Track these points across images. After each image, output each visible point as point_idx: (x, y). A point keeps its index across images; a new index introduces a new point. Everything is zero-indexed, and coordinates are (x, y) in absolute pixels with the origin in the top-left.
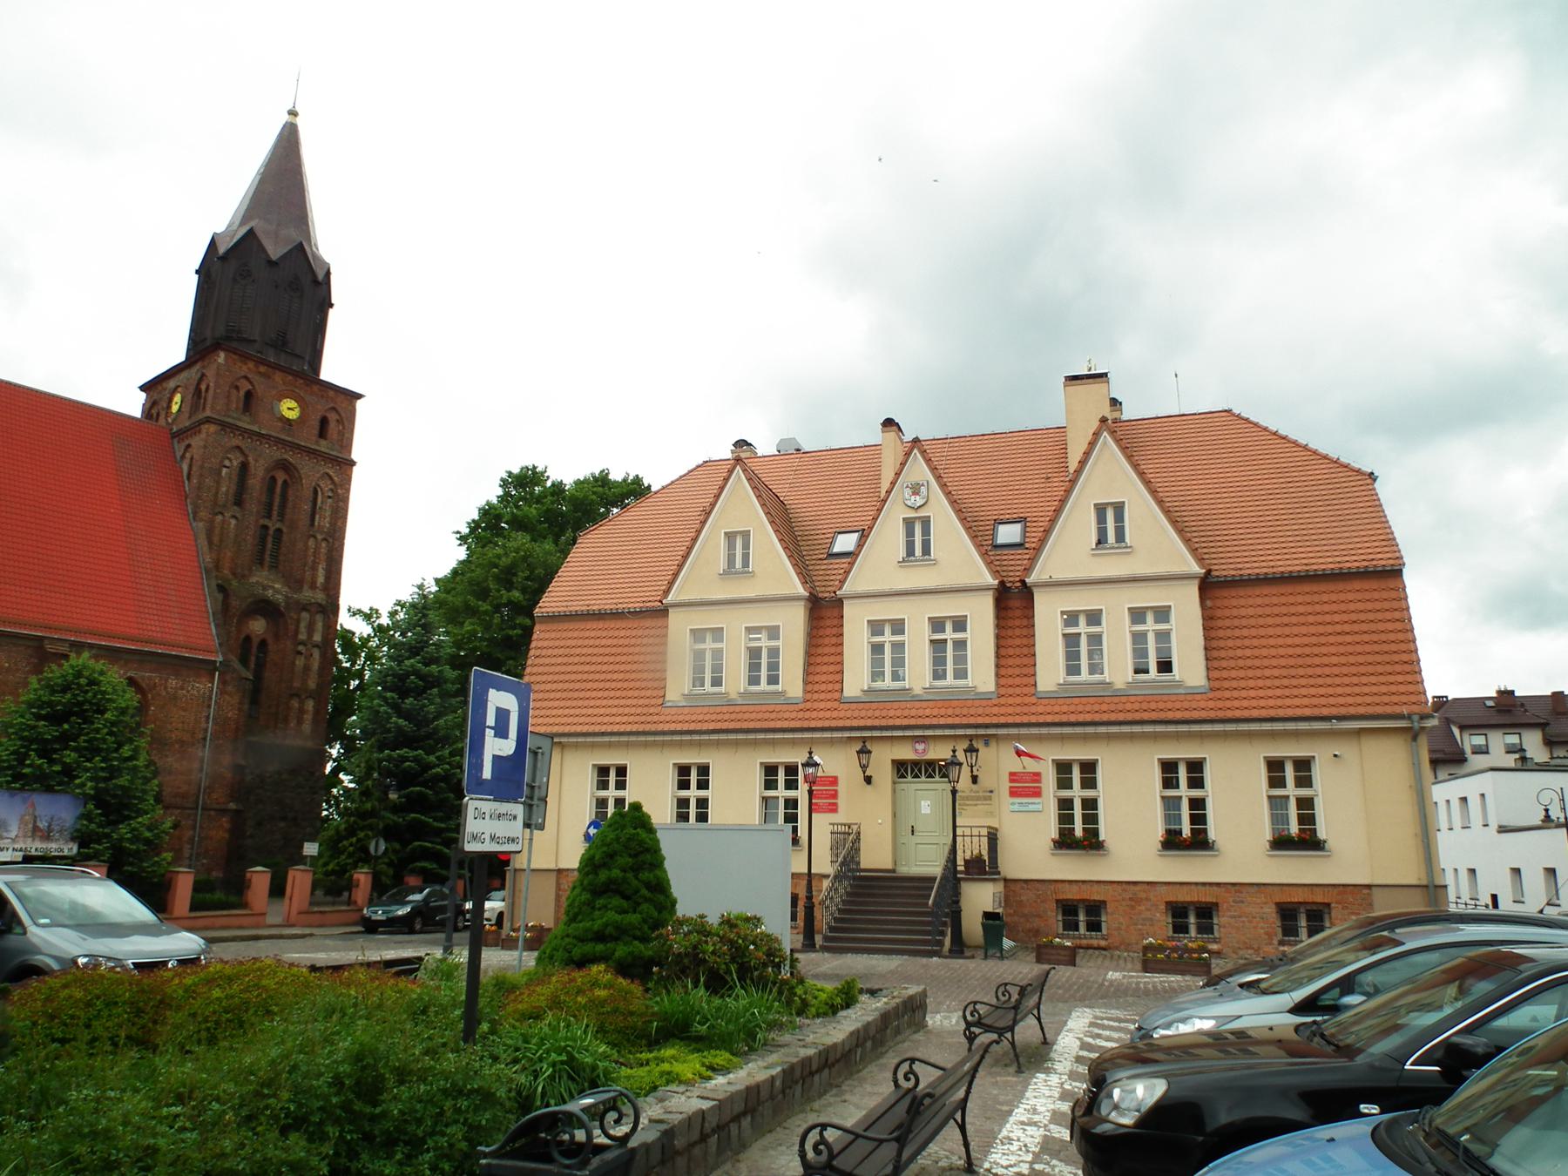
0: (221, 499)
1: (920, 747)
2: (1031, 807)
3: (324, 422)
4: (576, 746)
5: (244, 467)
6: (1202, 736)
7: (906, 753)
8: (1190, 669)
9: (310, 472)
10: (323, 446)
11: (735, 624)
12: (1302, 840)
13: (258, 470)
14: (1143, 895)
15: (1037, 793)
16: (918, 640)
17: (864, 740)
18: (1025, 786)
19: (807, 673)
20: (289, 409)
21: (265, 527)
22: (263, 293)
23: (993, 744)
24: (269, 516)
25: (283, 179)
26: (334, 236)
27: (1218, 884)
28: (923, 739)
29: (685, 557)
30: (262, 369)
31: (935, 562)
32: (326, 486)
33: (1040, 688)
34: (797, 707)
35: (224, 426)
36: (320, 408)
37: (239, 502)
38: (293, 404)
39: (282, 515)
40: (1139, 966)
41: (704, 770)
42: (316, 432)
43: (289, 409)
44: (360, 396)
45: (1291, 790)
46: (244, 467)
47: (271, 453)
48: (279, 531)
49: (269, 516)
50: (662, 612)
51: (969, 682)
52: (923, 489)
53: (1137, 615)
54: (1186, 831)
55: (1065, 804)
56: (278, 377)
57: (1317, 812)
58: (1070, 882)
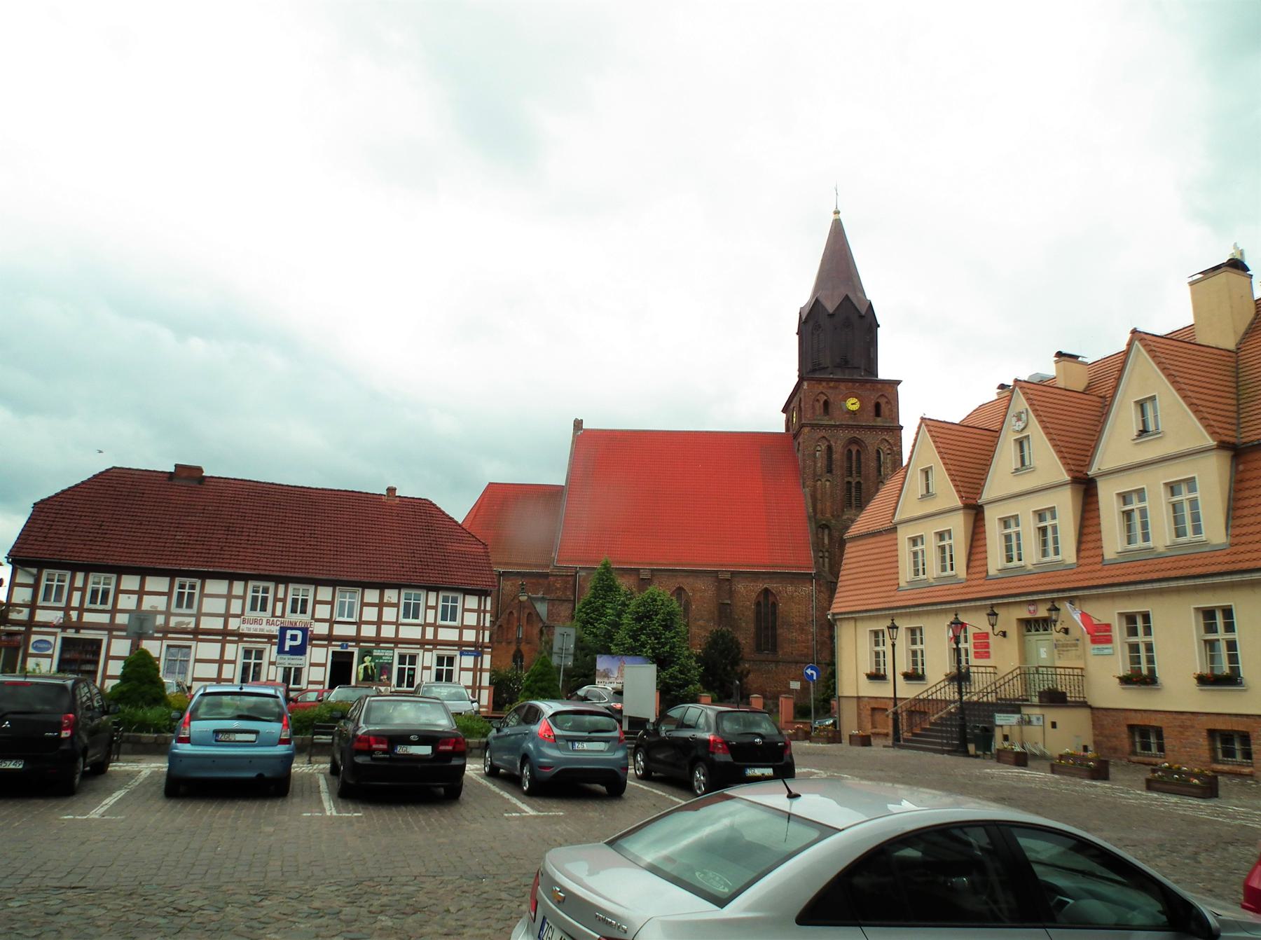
0: (819, 471)
1: (1032, 608)
2: (1106, 651)
3: (877, 407)
4: (863, 619)
5: (829, 448)
6: (918, 614)
7: (1024, 613)
8: (1215, 531)
9: (872, 441)
10: (879, 422)
11: (928, 530)
12: (1222, 679)
13: (838, 448)
14: (1188, 723)
15: (1108, 640)
16: (1028, 529)
17: (1053, 600)
18: (1100, 635)
19: (1080, 542)
20: (852, 404)
21: (849, 483)
22: (838, 334)
23: (1077, 603)
24: (851, 475)
25: (838, 261)
26: (877, 287)
27: (1247, 716)
28: (1033, 602)
29: (901, 490)
30: (832, 384)
31: (1034, 470)
32: (885, 448)
33: (1107, 557)
34: (1224, 552)
35: (813, 426)
36: (873, 397)
37: (830, 471)
38: (854, 400)
39: (859, 472)
40: (1049, 768)
41: (1228, 612)
42: (873, 414)
43: (852, 404)
44: (898, 382)
45: (1221, 635)
46: (829, 448)
47: (844, 435)
48: (859, 483)
49: (851, 475)
50: (893, 530)
51: (1203, 537)
52: (1023, 416)
53: (1173, 488)
54: (1145, 671)
55: (1134, 648)
56: (842, 386)
57: (1239, 652)
58: (1135, 711)
